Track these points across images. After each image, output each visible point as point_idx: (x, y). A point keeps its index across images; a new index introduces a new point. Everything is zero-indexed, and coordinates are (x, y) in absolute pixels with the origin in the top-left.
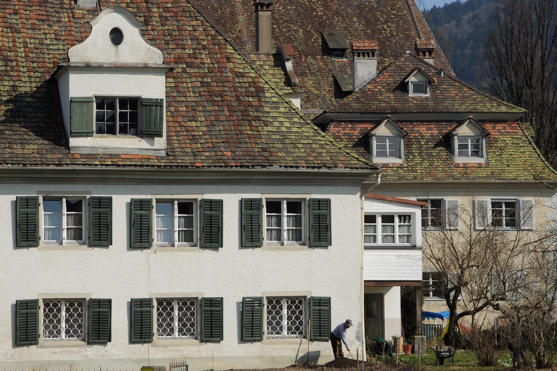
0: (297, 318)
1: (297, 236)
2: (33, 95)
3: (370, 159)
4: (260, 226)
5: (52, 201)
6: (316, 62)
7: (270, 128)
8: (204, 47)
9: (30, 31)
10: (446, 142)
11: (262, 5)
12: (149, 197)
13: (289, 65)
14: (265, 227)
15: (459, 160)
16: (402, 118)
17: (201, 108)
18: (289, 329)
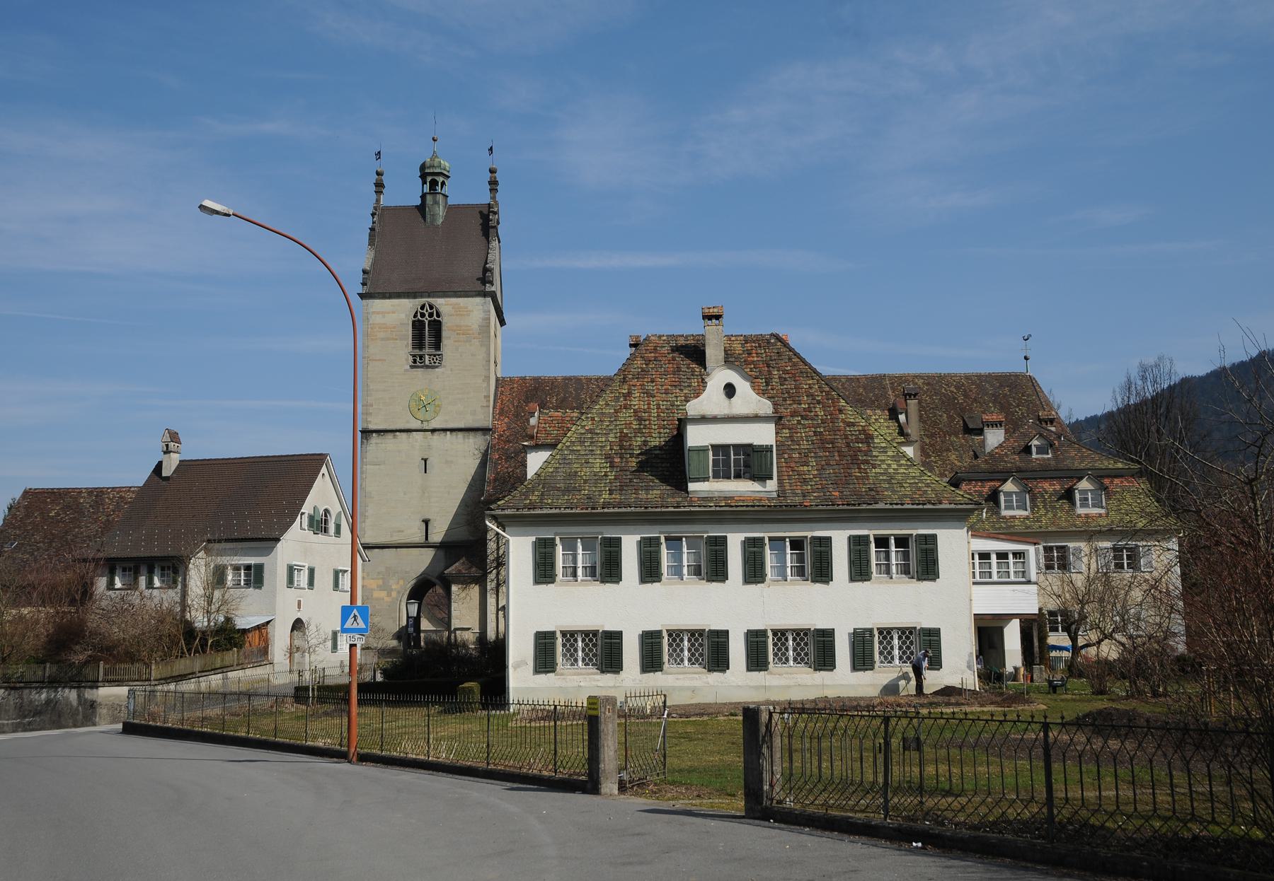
0: (908, 648)
1: (905, 570)
2: (660, 448)
3: (998, 513)
4: (868, 561)
5: (674, 541)
6: (959, 440)
7: (878, 470)
8: (819, 402)
10: (1068, 495)
11: (910, 395)
12: (761, 535)
13: (902, 418)
14: (874, 562)
15: (1081, 511)
16: (1027, 476)
18: (901, 658)
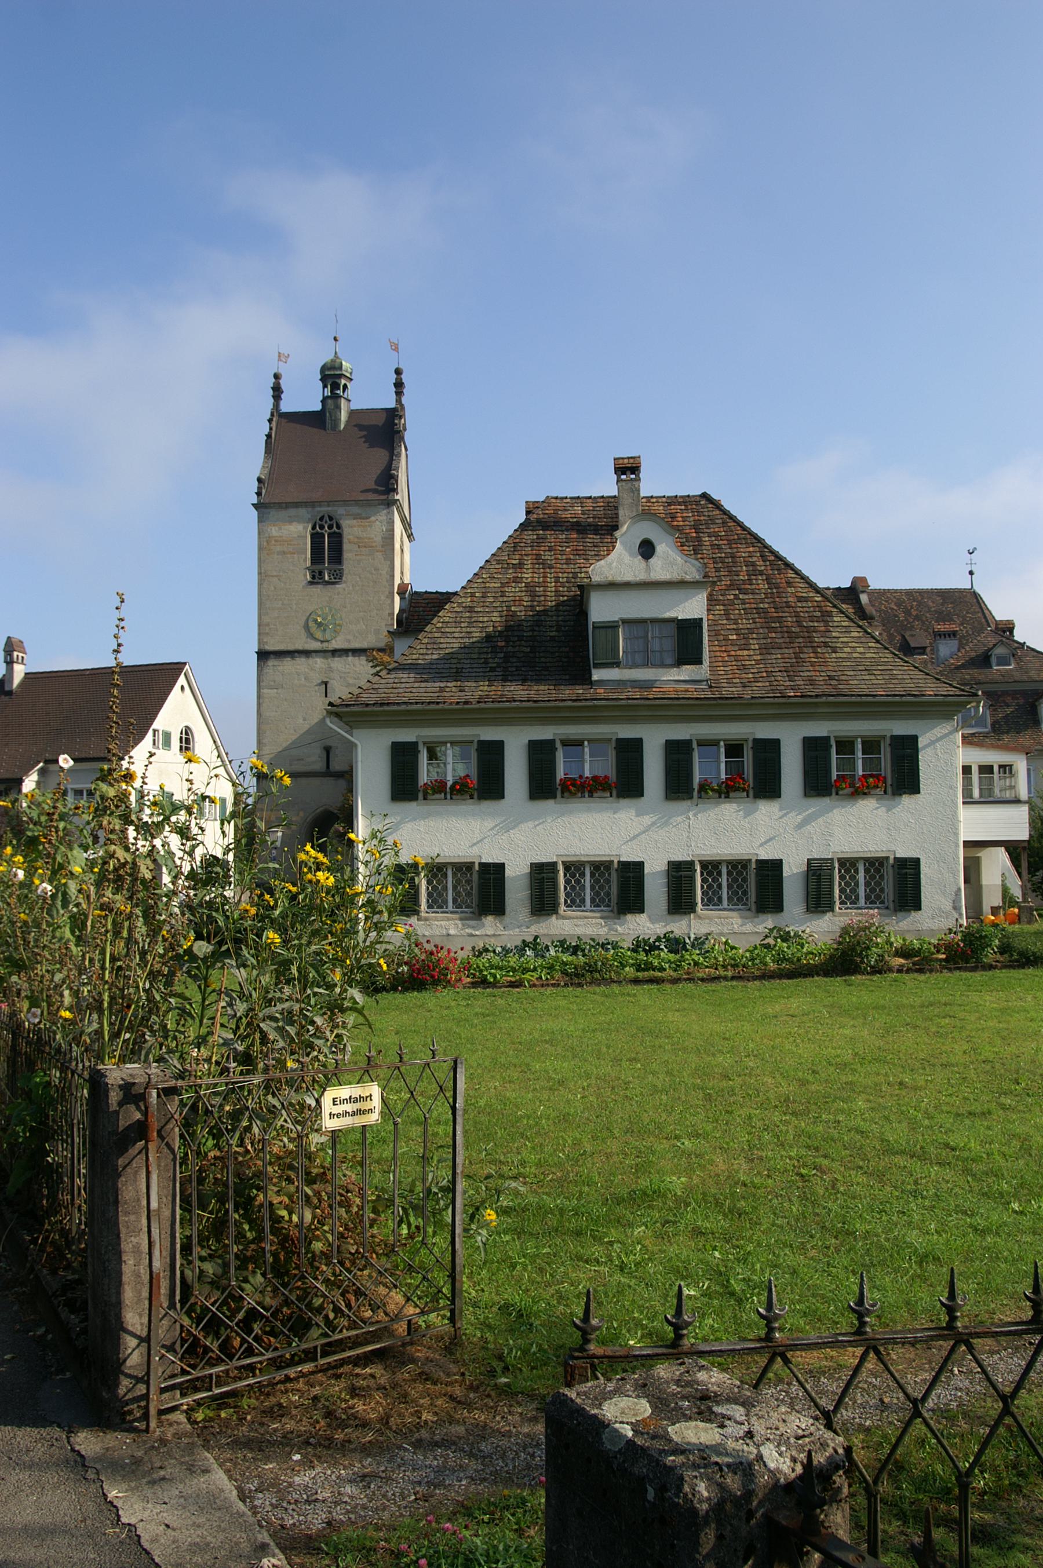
9: (565, 566)
17: (754, 636)
